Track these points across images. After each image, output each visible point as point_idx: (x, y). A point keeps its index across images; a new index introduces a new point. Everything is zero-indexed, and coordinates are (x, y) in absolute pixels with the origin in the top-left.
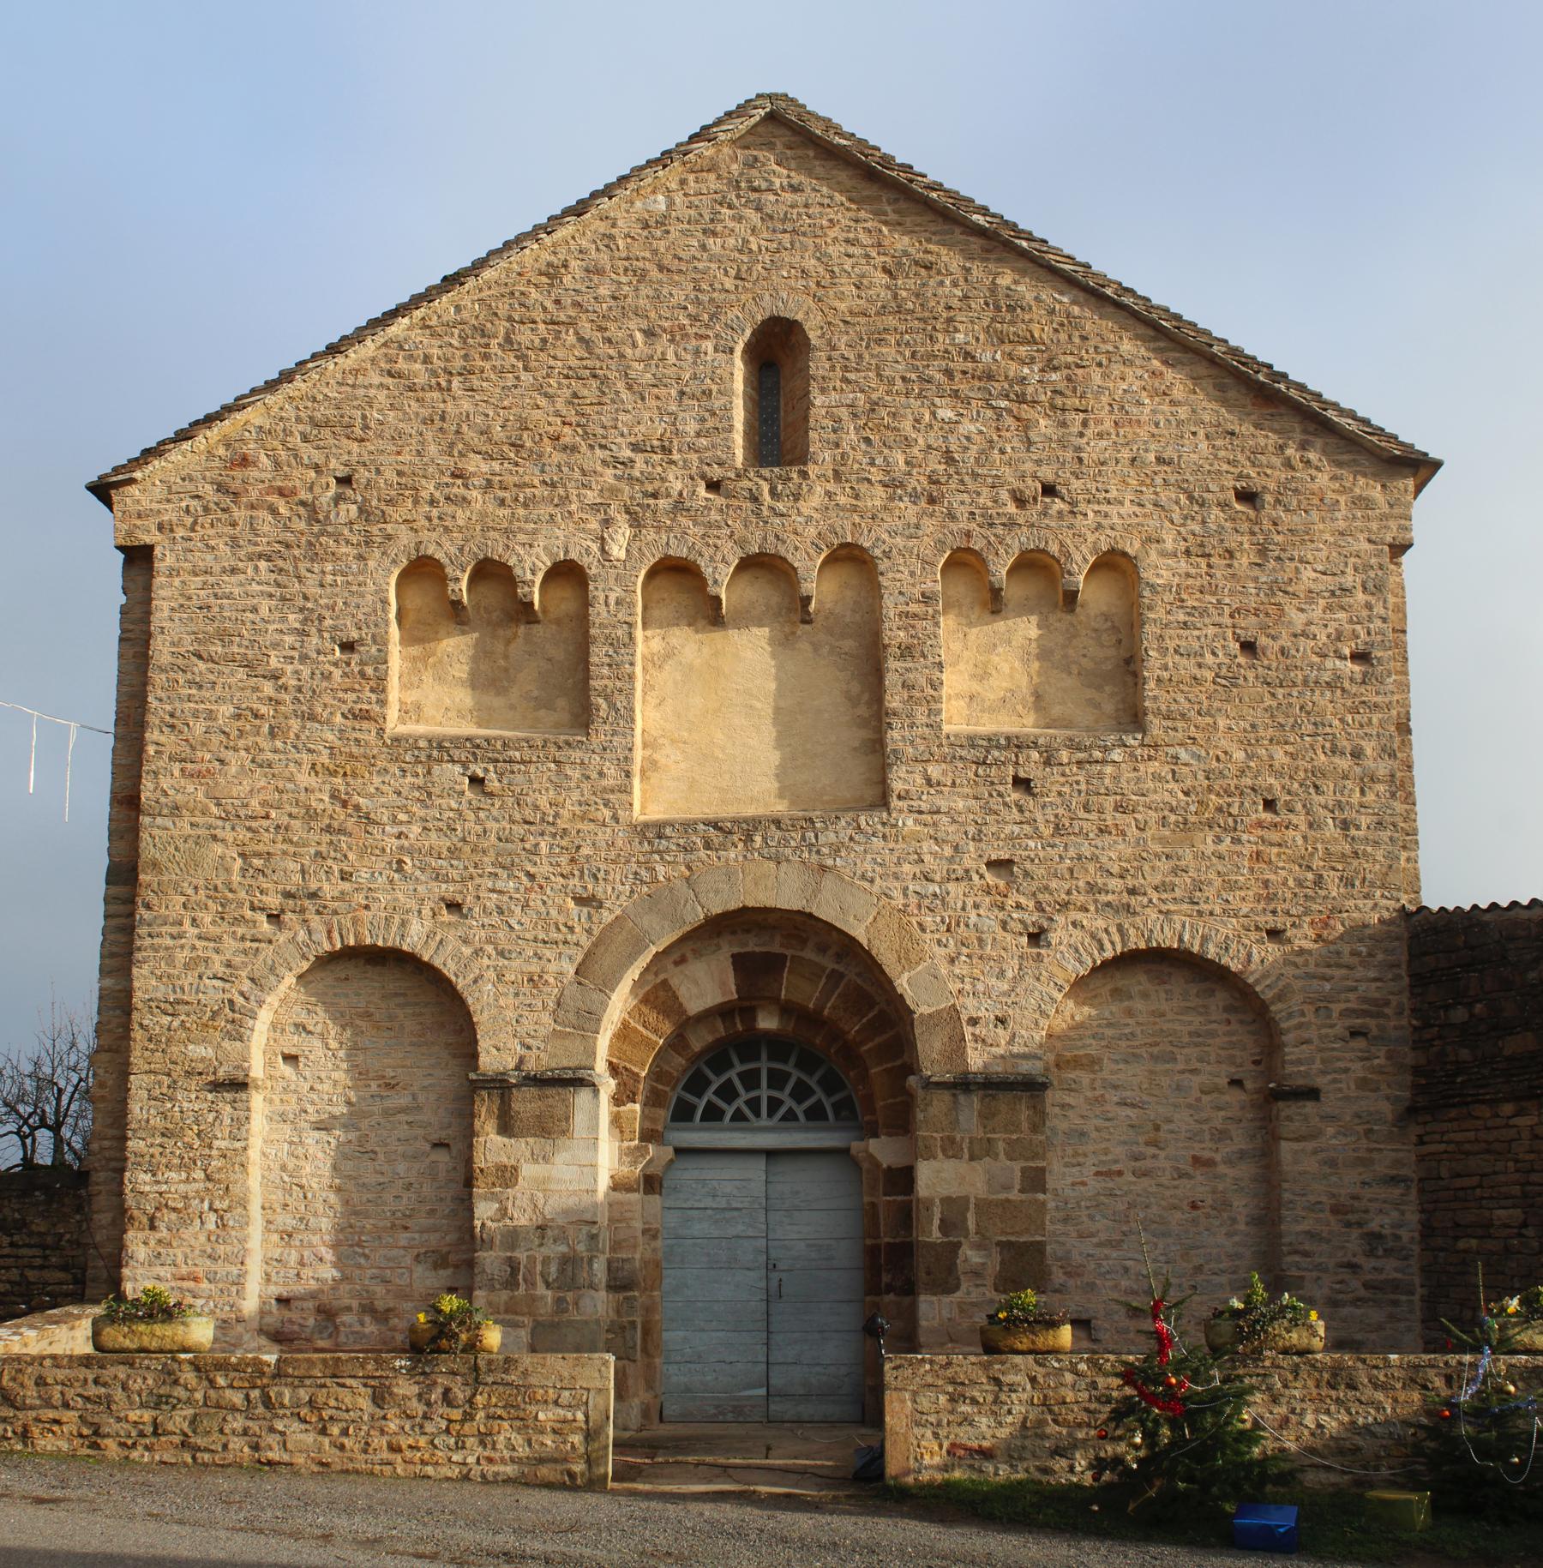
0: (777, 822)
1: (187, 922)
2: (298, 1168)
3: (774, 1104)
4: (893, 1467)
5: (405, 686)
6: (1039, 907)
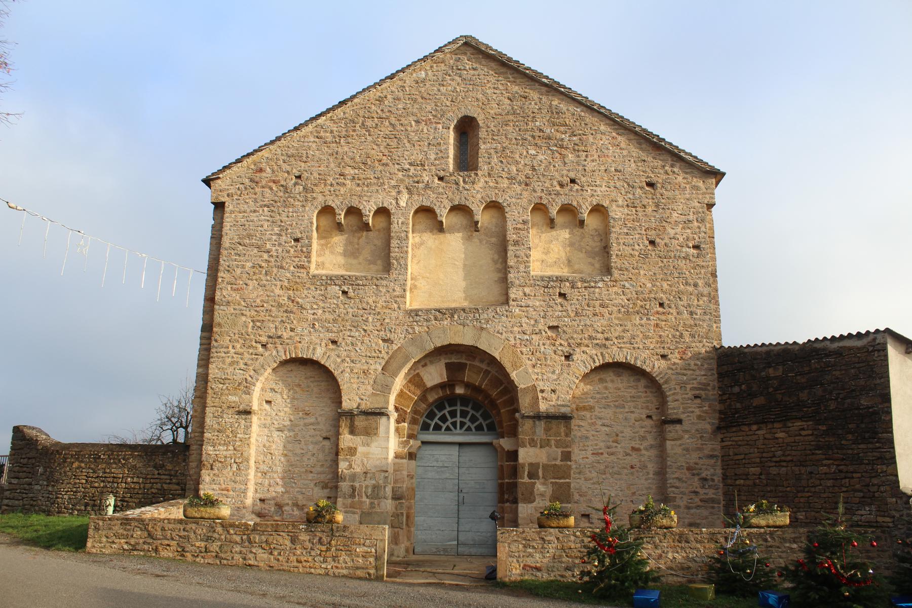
0: (464, 310)
1: (231, 347)
2: (270, 446)
3: (462, 424)
4: (500, 574)
5: (318, 256)
6: (569, 345)
